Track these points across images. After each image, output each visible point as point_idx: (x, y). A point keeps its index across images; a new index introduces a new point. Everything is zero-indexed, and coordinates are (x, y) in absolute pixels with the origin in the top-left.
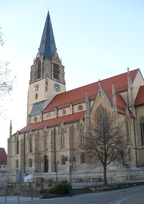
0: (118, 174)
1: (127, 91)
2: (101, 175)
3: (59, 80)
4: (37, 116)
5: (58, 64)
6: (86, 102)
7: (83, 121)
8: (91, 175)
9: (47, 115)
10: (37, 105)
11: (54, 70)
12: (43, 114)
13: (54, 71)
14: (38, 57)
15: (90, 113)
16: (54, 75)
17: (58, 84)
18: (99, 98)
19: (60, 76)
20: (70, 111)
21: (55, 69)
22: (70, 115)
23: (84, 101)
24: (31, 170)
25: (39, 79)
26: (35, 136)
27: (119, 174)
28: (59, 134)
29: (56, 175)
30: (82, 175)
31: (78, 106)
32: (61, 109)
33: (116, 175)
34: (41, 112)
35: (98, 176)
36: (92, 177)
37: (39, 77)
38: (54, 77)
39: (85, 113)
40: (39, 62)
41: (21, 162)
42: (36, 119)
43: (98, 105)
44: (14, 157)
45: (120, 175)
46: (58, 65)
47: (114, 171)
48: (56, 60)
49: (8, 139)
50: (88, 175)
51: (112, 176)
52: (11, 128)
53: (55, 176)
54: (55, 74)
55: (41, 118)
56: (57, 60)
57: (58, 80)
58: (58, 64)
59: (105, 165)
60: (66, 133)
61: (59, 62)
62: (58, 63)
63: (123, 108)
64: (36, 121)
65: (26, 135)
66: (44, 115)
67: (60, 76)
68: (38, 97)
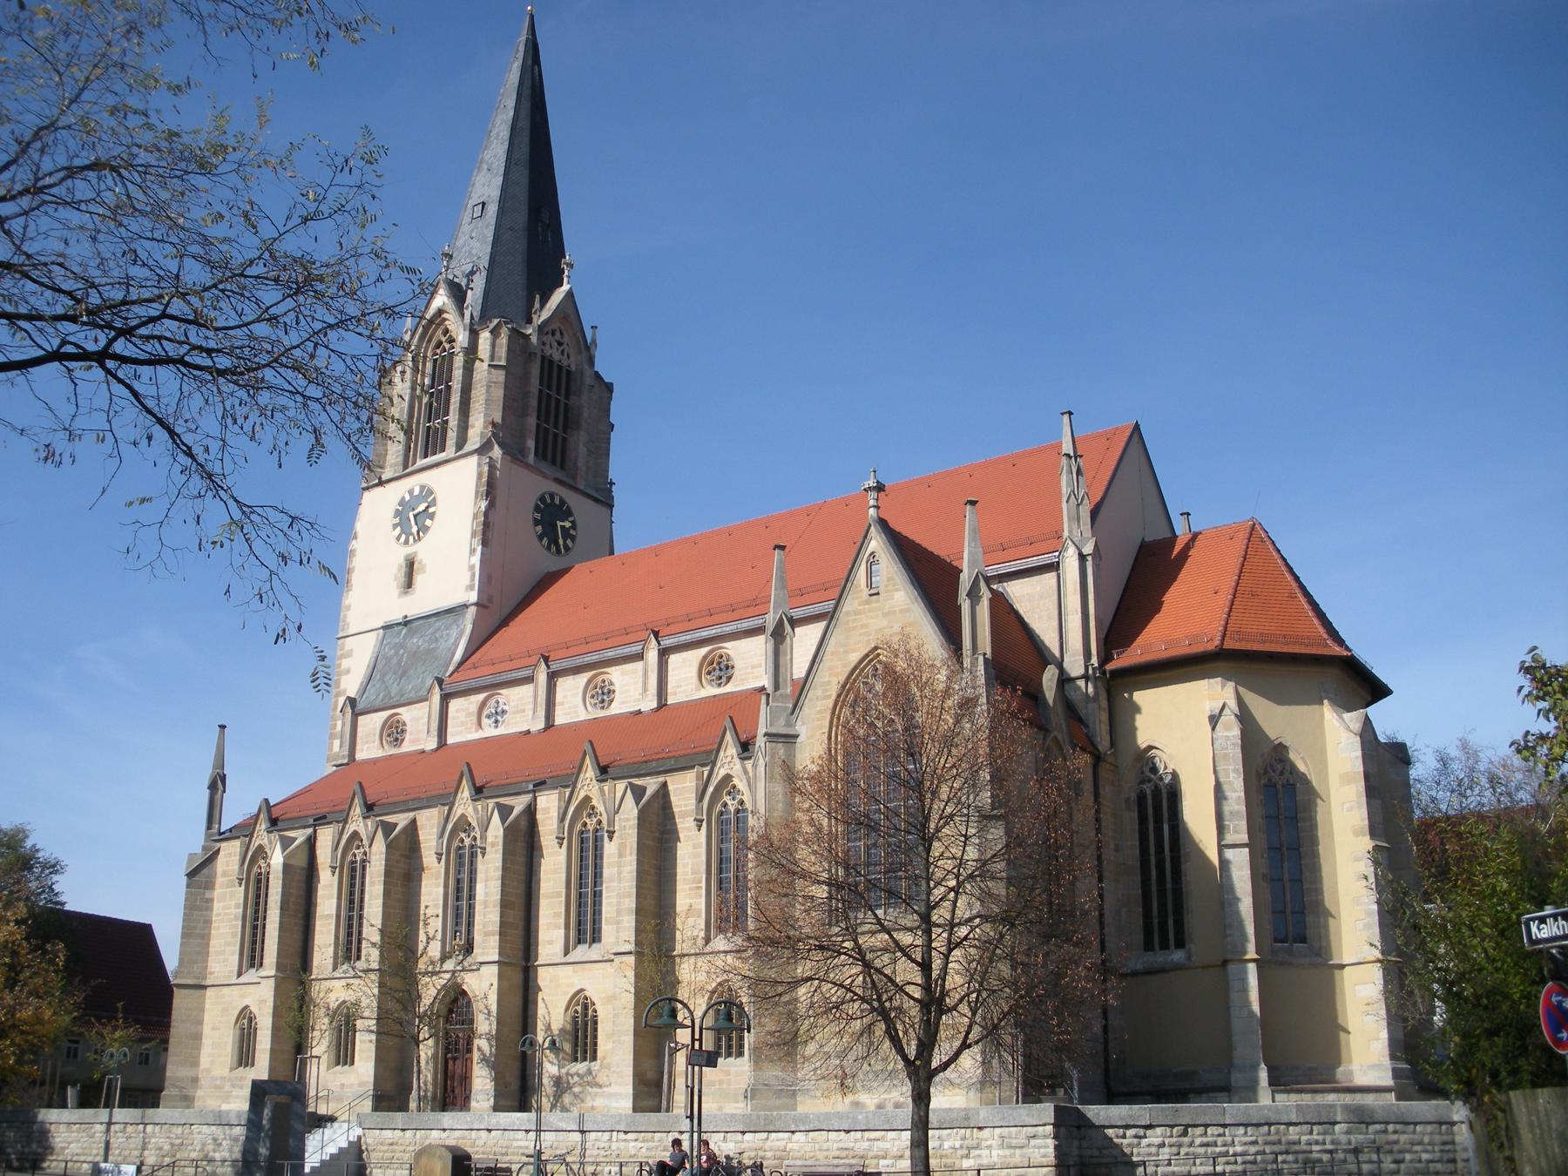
0: (989, 1147)
1: (1054, 567)
2: (866, 1144)
3: (574, 477)
4: (405, 714)
5: (572, 363)
6: (770, 628)
7: (743, 759)
8: (790, 1146)
9: (474, 708)
10: (410, 634)
11: (544, 400)
12: (446, 698)
13: (544, 413)
14: (440, 312)
15: (795, 706)
16: (542, 437)
17: (563, 502)
18: (867, 602)
19: (580, 444)
20: (645, 690)
21: (549, 396)
22: (639, 712)
23: (757, 622)
24: (342, 1086)
26: (388, 847)
27: (1002, 1146)
28: (561, 845)
29: (532, 1135)
30: (725, 1140)
31: (705, 658)
32: (577, 670)
33: (977, 1152)
34: (432, 687)
35: (844, 1154)
36: (798, 1163)
37: (434, 442)
38: (541, 453)
39: (764, 698)
40: (444, 339)
41: (276, 1029)
42: (394, 731)
43: (854, 651)
44: (225, 990)
45: (1007, 1152)
46: (569, 372)
47: (967, 1118)
48: (558, 334)
49: (192, 856)
50: (768, 1144)
51: (946, 1156)
52: (217, 784)
53: (527, 1143)
54: (546, 430)
55: (435, 725)
56: (566, 339)
57: (560, 475)
58: (573, 368)
59: (922, 1076)
60: (611, 834)
61: (580, 352)
62: (572, 358)
64: (397, 741)
65: (326, 836)
66: (455, 705)
67: (582, 450)
68: (419, 579)
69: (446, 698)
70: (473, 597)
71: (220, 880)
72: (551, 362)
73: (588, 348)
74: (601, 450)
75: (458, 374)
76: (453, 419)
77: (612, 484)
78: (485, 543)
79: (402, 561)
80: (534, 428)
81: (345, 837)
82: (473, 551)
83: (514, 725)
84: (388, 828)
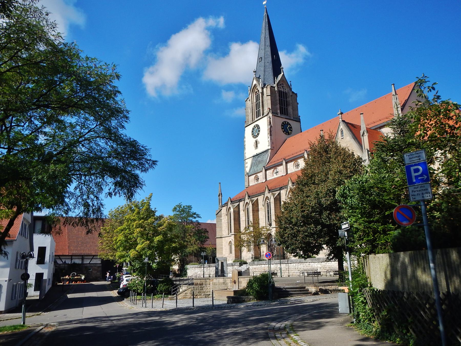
3: (290, 117)
4: (258, 174)
5: (287, 90)
10: (258, 157)
12: (266, 170)
13: (281, 103)
14: (255, 85)
16: (281, 109)
19: (290, 109)
25: (258, 118)
26: (252, 205)
37: (258, 115)
46: (286, 93)
55: (264, 177)
57: (287, 117)
63: (235, 283)
66: (268, 172)
68: (259, 145)
69: (266, 170)
70: (270, 147)
71: (223, 215)
72: (281, 92)
73: (289, 87)
74: (296, 109)
75: (261, 98)
76: (261, 109)
77: (300, 116)
78: (271, 135)
79: (254, 141)
80: (279, 108)
81: (245, 203)
82: (268, 138)
83: (280, 175)
84: (252, 201)
